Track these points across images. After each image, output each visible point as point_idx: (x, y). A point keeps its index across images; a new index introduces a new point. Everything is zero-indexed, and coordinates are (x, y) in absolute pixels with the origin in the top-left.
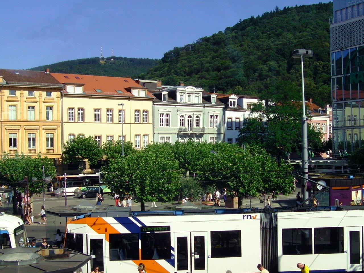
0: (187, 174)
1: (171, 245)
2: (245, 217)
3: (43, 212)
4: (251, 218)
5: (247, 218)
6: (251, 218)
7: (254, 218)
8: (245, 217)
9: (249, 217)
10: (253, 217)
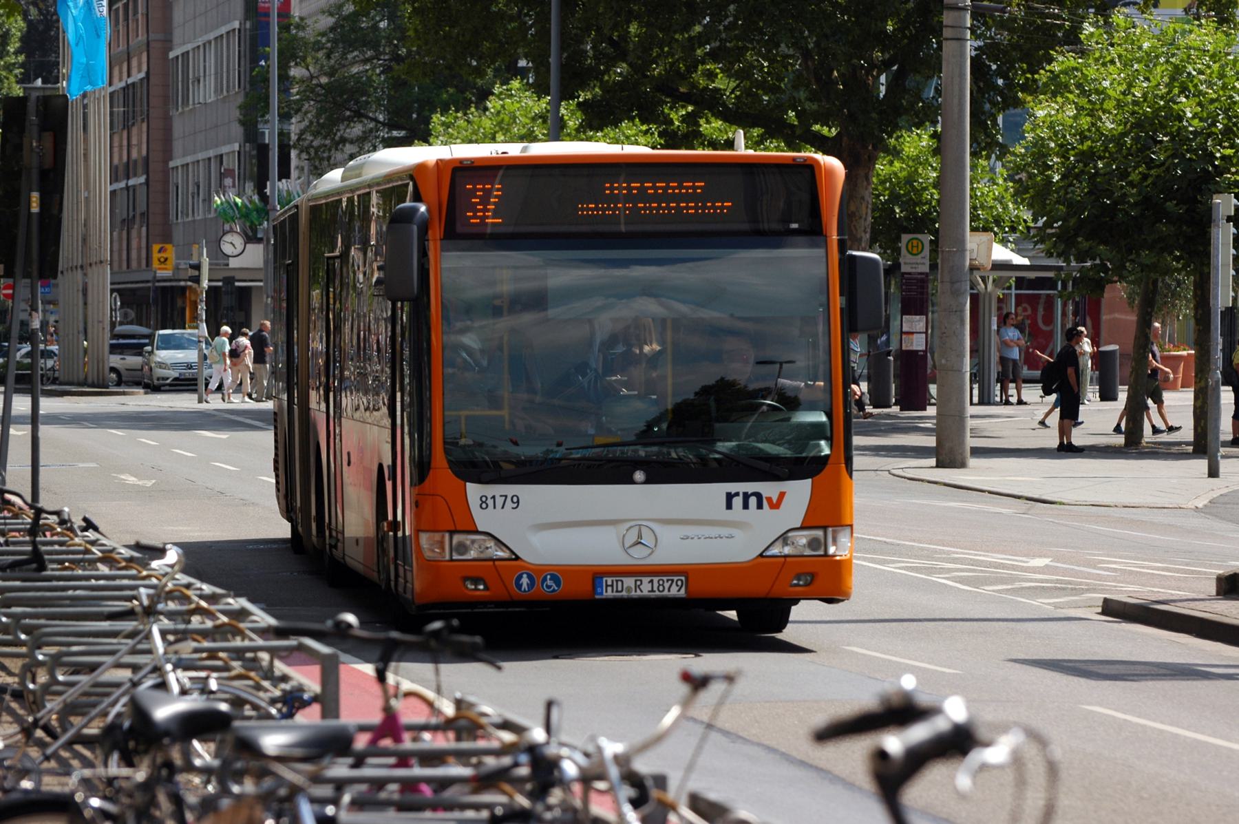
1: (793, 608)
2: (738, 502)
4: (760, 506)
5: (746, 506)
6: (760, 506)
7: (775, 505)
8: (738, 502)
9: (753, 501)
10: (769, 500)
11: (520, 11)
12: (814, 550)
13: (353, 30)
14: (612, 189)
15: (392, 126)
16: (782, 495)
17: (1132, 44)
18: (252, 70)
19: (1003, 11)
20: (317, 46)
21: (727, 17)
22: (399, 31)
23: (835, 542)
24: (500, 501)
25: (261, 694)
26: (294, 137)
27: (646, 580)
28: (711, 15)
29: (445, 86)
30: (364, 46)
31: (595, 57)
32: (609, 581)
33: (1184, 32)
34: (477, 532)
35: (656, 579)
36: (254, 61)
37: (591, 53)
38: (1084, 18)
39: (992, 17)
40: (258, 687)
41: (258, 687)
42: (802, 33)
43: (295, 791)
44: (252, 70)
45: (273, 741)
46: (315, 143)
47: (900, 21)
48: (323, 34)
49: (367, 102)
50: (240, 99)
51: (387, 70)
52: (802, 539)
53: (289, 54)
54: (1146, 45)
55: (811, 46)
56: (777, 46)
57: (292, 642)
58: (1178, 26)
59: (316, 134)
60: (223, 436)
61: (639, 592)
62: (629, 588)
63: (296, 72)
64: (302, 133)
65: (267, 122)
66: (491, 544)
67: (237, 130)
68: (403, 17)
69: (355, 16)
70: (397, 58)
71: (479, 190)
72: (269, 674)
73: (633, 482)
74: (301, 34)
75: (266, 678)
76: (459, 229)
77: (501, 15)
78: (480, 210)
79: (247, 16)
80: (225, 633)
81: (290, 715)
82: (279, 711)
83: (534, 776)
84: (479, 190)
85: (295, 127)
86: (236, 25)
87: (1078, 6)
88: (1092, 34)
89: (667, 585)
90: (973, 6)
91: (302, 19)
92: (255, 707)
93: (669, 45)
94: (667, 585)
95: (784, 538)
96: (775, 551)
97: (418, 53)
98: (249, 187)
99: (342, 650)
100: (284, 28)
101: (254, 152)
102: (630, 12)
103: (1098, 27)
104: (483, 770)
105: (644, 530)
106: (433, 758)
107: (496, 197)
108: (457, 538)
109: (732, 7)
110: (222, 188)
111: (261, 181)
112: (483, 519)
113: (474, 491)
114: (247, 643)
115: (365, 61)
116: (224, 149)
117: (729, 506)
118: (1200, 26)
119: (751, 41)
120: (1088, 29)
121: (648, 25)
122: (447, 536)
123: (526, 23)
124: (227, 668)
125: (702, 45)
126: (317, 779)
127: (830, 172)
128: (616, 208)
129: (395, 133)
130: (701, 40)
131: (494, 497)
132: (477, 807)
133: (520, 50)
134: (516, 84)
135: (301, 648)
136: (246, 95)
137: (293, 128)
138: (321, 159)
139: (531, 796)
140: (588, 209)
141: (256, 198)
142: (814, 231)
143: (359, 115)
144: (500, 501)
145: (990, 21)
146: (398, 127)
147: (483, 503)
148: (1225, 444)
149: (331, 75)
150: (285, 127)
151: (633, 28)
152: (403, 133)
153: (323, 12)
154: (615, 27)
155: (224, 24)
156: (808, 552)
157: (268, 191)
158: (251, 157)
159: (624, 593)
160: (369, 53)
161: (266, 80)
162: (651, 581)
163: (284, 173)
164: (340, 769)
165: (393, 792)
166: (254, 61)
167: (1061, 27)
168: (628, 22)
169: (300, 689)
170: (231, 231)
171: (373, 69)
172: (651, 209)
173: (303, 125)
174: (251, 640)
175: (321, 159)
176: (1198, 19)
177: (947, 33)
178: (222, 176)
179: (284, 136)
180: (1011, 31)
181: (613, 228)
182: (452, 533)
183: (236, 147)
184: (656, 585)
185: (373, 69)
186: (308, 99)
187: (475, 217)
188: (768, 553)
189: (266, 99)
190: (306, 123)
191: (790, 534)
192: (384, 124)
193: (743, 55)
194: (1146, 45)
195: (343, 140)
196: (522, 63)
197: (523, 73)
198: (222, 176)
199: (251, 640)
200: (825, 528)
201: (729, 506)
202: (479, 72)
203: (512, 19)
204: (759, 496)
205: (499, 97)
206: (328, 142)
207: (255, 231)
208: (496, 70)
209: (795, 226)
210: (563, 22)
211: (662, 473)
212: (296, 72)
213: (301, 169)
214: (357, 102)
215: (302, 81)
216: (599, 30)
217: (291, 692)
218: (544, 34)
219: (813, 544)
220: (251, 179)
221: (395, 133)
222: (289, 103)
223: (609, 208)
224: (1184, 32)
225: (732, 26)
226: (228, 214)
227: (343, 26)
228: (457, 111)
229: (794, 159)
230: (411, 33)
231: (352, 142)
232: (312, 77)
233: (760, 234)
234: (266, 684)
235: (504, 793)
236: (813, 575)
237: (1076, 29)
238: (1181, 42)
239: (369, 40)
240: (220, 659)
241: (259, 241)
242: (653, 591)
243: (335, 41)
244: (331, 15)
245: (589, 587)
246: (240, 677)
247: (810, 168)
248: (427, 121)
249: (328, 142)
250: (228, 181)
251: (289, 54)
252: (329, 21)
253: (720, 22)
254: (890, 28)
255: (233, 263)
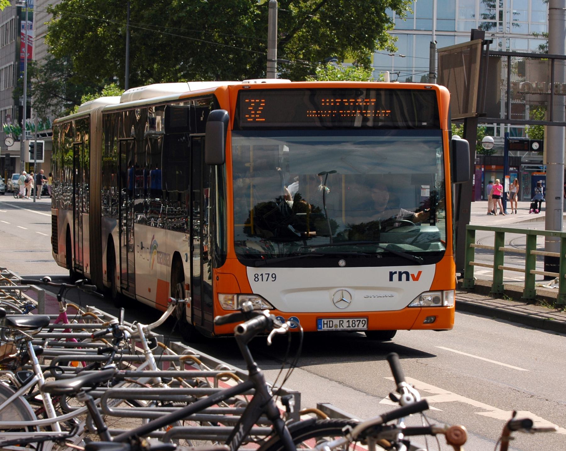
0: (458, 137)
2: (396, 277)
3: (179, 202)
4: (408, 279)
5: (400, 279)
6: (408, 279)
7: (416, 279)
8: (396, 277)
9: (404, 276)
10: (413, 275)
11: (114, 60)
12: (436, 303)
13: (54, 65)
14: (325, 102)
15: (67, 100)
16: (420, 273)
17: (334, 75)
18: (18, 79)
19: (288, 62)
20: (41, 71)
21: (189, 62)
22: (70, 65)
23: (447, 298)
24: (265, 277)
25: (17, 305)
26: (32, 103)
27: (345, 320)
28: (183, 62)
29: (87, 85)
30: (58, 71)
31: (142, 76)
32: (325, 321)
33: (352, 71)
34: (252, 294)
35: (351, 320)
36: (18, 76)
37: (140, 74)
38: (317, 65)
39: (285, 64)
40: (16, 302)
41: (16, 302)
42: (216, 68)
43: (28, 339)
44: (18, 79)
45: (20, 321)
46: (40, 106)
47: (252, 65)
48: (43, 67)
49: (59, 91)
50: (13, 89)
51: (66, 80)
52: (429, 297)
53: (31, 74)
54: (339, 76)
55: (219, 73)
56: (207, 73)
57: (28, 286)
58: (350, 69)
59: (40, 102)
60: (5, 211)
61: (341, 327)
62: (336, 325)
63: (33, 80)
64: (35, 102)
65: (22, 98)
66: (260, 301)
67: (12, 101)
68: (72, 61)
69: (55, 60)
70: (70, 76)
71: (253, 103)
72: (19, 298)
73: (339, 266)
74: (35, 66)
75: (18, 299)
76: (241, 124)
77: (107, 60)
78: (253, 114)
79: (16, 61)
80: (4, 282)
81: (27, 313)
82: (23, 311)
83: (114, 336)
84: (253, 103)
85: (32, 100)
86: (12, 63)
87: (315, 61)
88: (320, 71)
89: (357, 323)
90: (278, 60)
91: (36, 61)
92: (14, 309)
93: (168, 72)
94: (357, 323)
95: (420, 297)
96: (416, 303)
97: (77, 74)
98: (16, 121)
99: (46, 289)
100: (29, 64)
101: (18, 109)
102: (154, 60)
103: (322, 69)
104: (95, 333)
105: (345, 293)
106: (77, 329)
107: (251, 106)
108: (241, 298)
109: (191, 59)
110: (6, 121)
111: (20, 120)
112: (256, 287)
113: (251, 271)
114: (12, 286)
115: (58, 76)
116: (7, 108)
117: (391, 279)
118: (358, 69)
119: (198, 71)
120: (318, 69)
121: (161, 65)
122: (235, 296)
123: (116, 63)
124: (4, 295)
125: (180, 72)
126: (35, 336)
127: (443, 95)
128: (327, 113)
129: (68, 102)
130: (180, 70)
131: (262, 275)
132: (94, 347)
133: (114, 73)
134: (112, 85)
135: (31, 288)
136: (15, 88)
137: (32, 100)
138: (42, 112)
139: (113, 343)
140: (312, 114)
141: (18, 125)
142: (435, 127)
143: (56, 96)
144: (265, 277)
145: (284, 66)
146: (70, 101)
147: (256, 277)
148: (541, 233)
149: (46, 81)
150: (29, 100)
151: (155, 66)
152: (71, 103)
153: (43, 59)
154: (149, 65)
155: (8, 62)
156: (433, 304)
157: (22, 123)
158: (17, 110)
159: (333, 328)
160: (60, 74)
161: (23, 83)
162: (349, 321)
163: (28, 116)
164: (44, 332)
165: (64, 341)
166: (18, 76)
167: (309, 68)
168: (153, 64)
169: (31, 303)
170: (8, 137)
171: (61, 79)
172: (347, 114)
173: (35, 99)
174: (13, 285)
175: (42, 112)
176: (357, 66)
177: (268, 70)
178: (6, 117)
179: (28, 103)
180: (291, 69)
181: (312, 124)
182: (238, 295)
183: (11, 107)
184: (351, 323)
185: (61, 79)
186: (37, 90)
187: (250, 117)
188: (412, 305)
189: (22, 90)
190: (37, 98)
191: (423, 294)
192: (64, 99)
193: (195, 76)
194: (339, 76)
195: (50, 105)
196: (115, 78)
197: (115, 81)
198: (6, 117)
199: (13, 285)
200: (442, 291)
201: (391, 279)
202: (99, 81)
203: (111, 62)
204: (407, 273)
205: (106, 89)
206: (44, 105)
207: (17, 137)
208: (106, 80)
209: (425, 124)
210: (130, 63)
211: (354, 261)
212: (33, 80)
213: (34, 115)
214: (55, 91)
215: (35, 83)
216: (143, 66)
217: (27, 304)
218: (123, 67)
219: (436, 300)
220: (16, 118)
221: (68, 102)
222: (31, 91)
223: (324, 113)
224: (352, 71)
225: (191, 66)
226: (7, 131)
227: (50, 64)
228: (91, 94)
229: (425, 87)
230: (75, 66)
231: (53, 106)
232: (39, 82)
233: (411, 129)
234: (18, 301)
235: (104, 342)
236: (435, 317)
237: (314, 69)
238: (351, 75)
239: (60, 69)
240: (2, 292)
241: (19, 141)
242: (349, 326)
243: (47, 69)
244: (46, 60)
245: (315, 325)
246: (9, 298)
247: (434, 92)
248: (80, 98)
249: (44, 105)
250: (8, 119)
251: (31, 74)
252: (46, 62)
253: (187, 64)
254: (248, 67)
255: (9, 149)
